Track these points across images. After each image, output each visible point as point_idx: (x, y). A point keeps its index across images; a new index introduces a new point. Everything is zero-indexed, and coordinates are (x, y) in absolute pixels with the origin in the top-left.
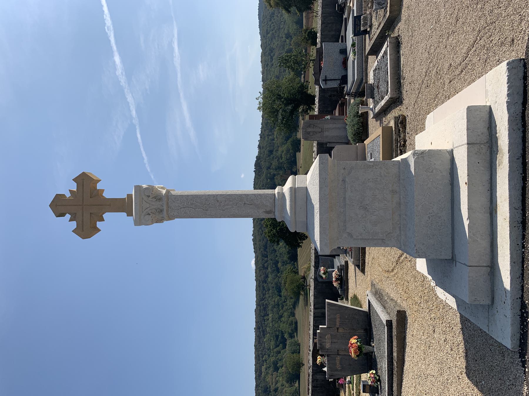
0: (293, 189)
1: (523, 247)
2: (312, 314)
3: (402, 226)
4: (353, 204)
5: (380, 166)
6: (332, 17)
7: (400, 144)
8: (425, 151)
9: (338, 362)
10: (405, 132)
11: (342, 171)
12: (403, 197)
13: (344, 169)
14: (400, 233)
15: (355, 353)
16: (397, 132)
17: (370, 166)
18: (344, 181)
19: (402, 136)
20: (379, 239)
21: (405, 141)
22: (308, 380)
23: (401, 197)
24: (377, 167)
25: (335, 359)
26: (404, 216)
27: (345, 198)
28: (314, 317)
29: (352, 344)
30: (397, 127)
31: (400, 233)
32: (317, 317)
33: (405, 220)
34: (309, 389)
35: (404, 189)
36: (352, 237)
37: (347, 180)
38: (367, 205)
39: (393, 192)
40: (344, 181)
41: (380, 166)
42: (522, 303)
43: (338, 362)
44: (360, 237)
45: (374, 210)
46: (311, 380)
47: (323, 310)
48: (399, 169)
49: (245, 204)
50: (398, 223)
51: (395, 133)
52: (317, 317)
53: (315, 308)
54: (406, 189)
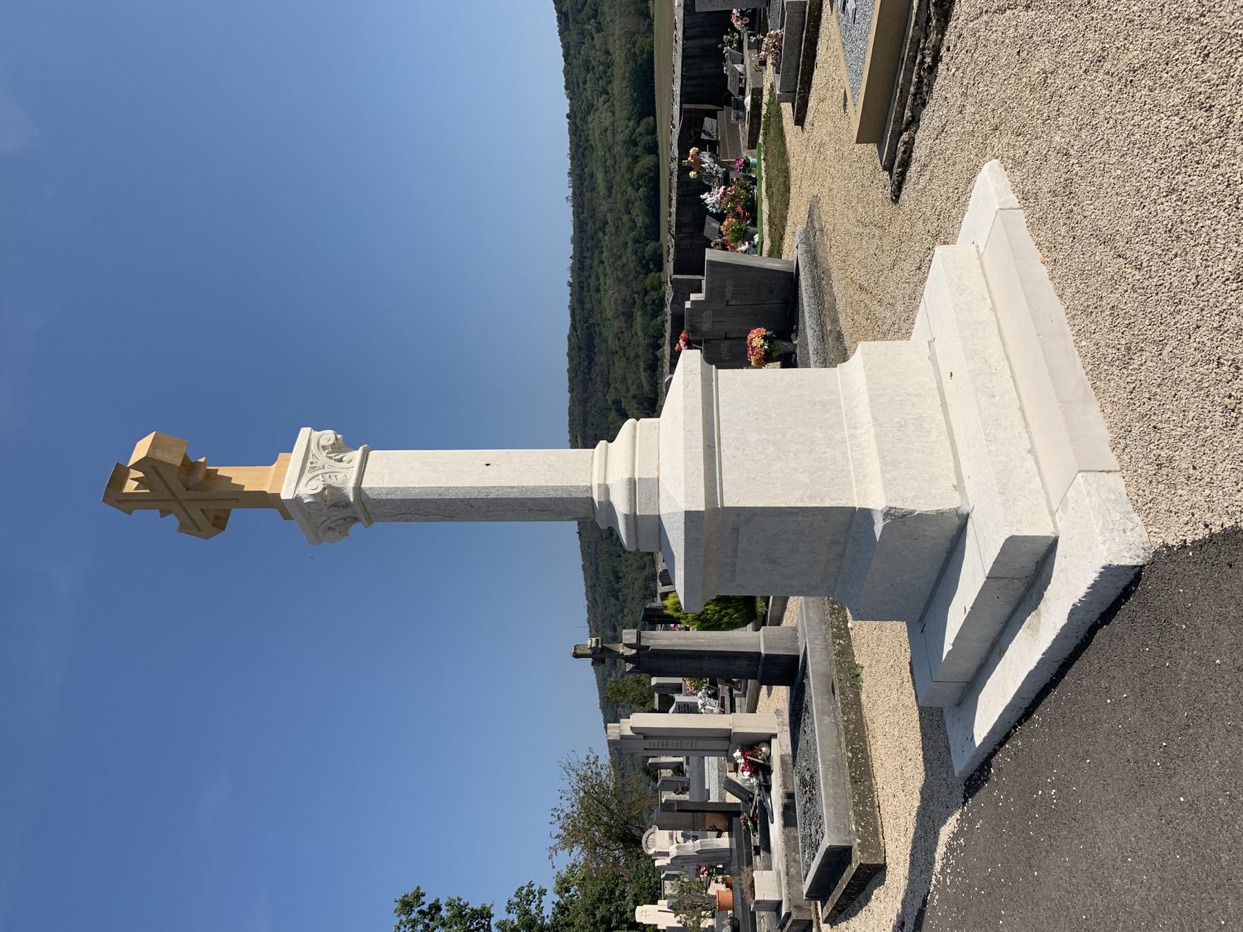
0: (632, 519)
1: (1015, 727)
2: (680, 50)
7: (922, 62)
8: (912, 512)
10: (942, 30)
16: (923, 18)
19: (933, 36)
21: (937, 58)
22: (670, 183)
27: (735, 549)
28: (684, 58)
29: (753, 348)
30: (924, 7)
32: (692, 57)
34: (670, 199)
40: (736, 529)
42: (982, 765)
46: (675, 185)
47: (699, 277)
49: (530, 510)
51: (916, 23)
52: (692, 57)
53: (685, 38)
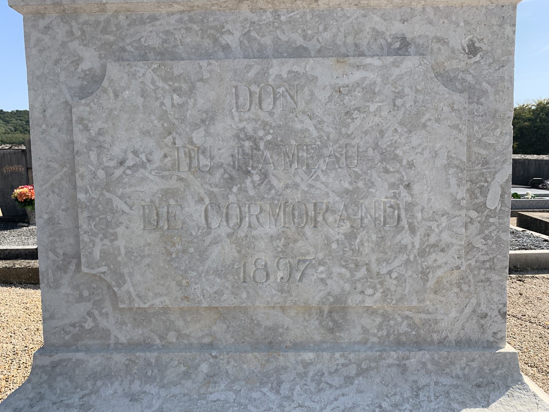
3: (152, 356)
4: (268, 103)
5: (479, 242)
6: (522, 172)
9: (15, 168)
11: (459, 40)
12: (306, 365)
13: (472, 50)
14: (119, 347)
15: (21, 194)
17: (484, 191)
18: (403, 46)
20: (77, 236)
23: (309, 356)
24: (474, 228)
25: (19, 164)
26: (204, 368)
27: (300, 53)
31: (119, 347)
33: (186, 375)
35: (353, 370)
36: (84, 93)
37: (410, 63)
38: (265, 176)
39: (335, 314)
40: (403, 46)
41: (479, 242)
43: (15, 168)
44: (80, 138)
45: (235, 212)
48: (459, 344)
50: (172, 337)
54: (349, 380)
